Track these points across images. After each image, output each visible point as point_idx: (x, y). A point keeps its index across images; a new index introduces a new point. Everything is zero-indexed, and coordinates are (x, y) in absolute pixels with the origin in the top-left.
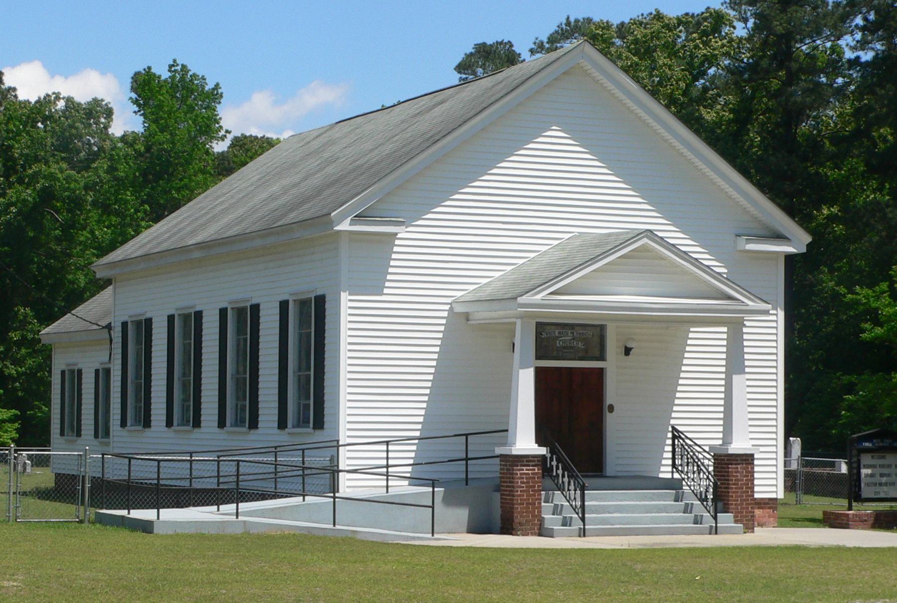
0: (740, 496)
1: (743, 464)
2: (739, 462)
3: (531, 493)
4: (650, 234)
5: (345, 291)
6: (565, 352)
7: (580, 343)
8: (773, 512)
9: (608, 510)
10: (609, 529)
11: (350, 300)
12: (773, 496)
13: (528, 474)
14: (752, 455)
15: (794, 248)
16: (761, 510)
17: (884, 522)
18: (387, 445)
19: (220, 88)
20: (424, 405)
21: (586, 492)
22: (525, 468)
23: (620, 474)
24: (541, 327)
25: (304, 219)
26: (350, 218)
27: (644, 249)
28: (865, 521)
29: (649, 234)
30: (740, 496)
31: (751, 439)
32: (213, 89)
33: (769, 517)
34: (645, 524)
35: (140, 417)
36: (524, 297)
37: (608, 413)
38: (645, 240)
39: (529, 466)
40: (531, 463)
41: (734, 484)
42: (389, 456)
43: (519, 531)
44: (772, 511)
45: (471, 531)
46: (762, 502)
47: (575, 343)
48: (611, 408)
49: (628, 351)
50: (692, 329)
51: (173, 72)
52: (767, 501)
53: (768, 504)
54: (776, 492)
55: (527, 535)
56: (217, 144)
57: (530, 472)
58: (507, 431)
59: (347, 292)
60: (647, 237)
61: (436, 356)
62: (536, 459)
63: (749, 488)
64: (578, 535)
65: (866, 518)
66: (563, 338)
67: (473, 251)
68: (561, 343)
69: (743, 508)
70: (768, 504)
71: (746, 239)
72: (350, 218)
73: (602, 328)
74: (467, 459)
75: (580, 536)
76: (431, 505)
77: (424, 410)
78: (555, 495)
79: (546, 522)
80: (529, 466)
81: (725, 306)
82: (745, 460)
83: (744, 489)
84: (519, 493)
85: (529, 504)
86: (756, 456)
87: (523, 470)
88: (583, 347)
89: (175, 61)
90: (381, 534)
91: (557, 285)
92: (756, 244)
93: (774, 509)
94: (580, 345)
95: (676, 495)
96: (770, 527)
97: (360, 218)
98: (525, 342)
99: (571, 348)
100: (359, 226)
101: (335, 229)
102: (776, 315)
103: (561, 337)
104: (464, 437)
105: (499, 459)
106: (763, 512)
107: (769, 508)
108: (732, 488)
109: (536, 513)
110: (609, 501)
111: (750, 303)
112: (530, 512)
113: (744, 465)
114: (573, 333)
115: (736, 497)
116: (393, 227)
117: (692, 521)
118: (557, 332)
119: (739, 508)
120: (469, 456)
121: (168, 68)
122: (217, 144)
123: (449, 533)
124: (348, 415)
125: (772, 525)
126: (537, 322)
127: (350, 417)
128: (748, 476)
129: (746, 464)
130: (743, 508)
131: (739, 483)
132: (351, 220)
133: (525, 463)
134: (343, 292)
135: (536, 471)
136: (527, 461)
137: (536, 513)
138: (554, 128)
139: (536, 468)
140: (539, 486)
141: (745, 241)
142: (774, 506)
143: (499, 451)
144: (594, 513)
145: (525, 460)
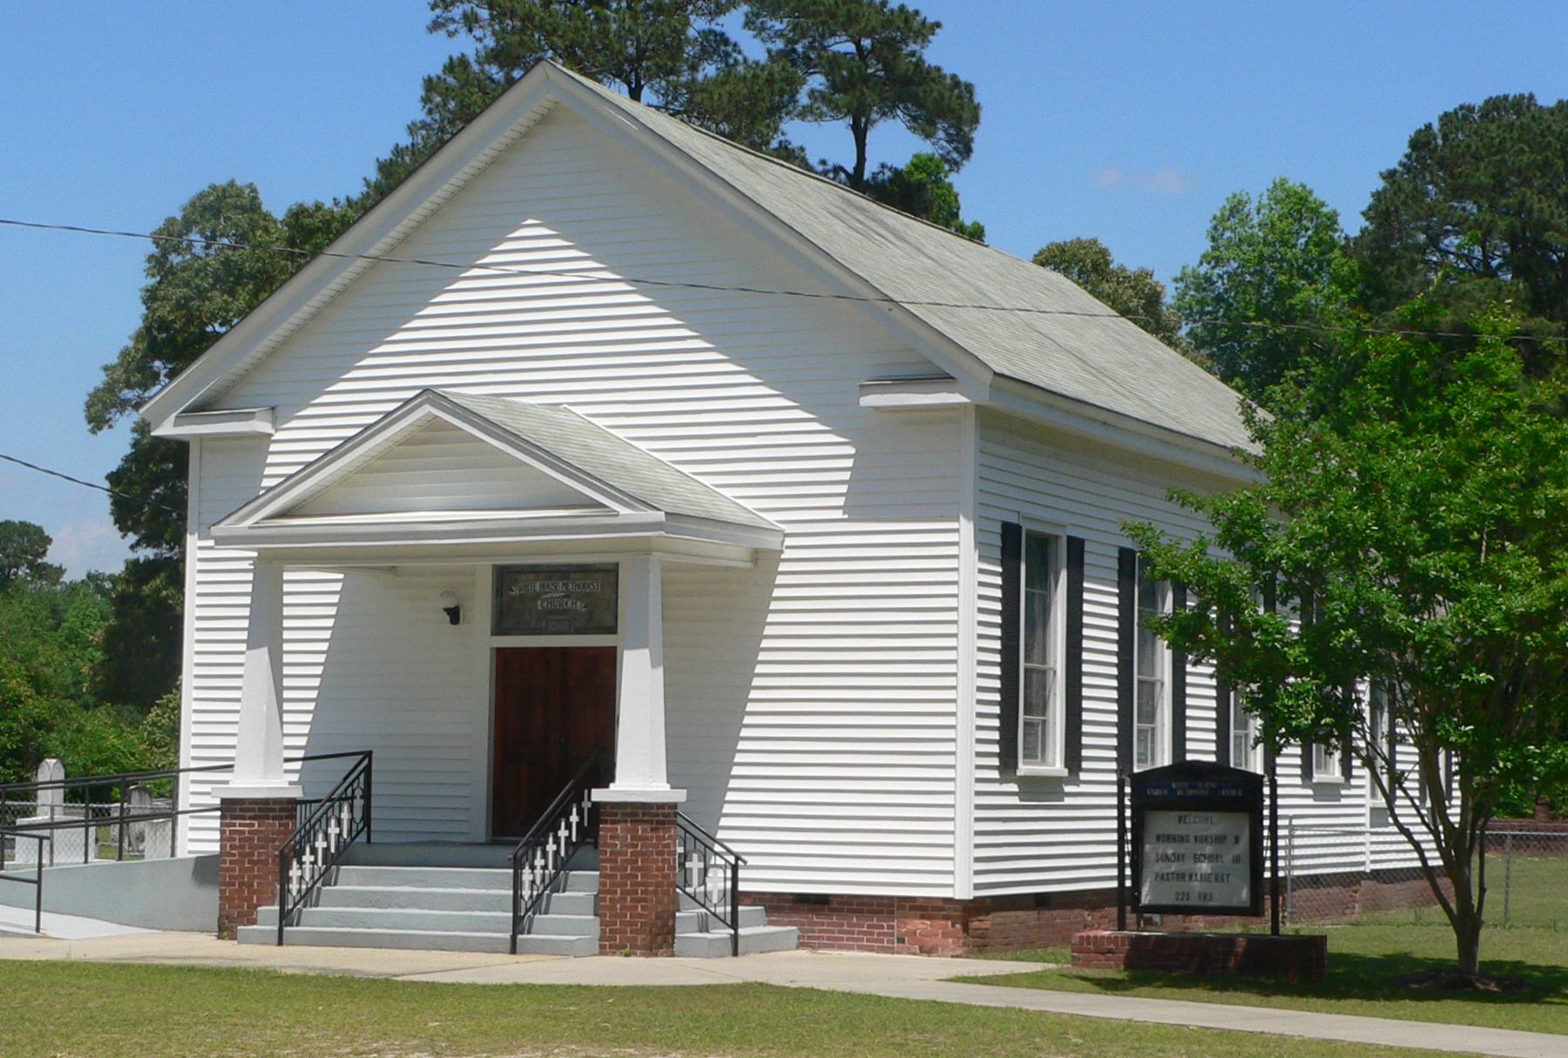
0: (619, 885)
1: (626, 821)
2: (619, 818)
3: (247, 865)
5: (192, 534)
7: (578, 603)
8: (953, 925)
11: (201, 548)
15: (965, 396)
22: (238, 822)
24: (505, 576)
25: (1053, 389)
26: (174, 415)
27: (433, 425)
28: (1110, 951)
33: (945, 935)
34: (426, 930)
35: (1237, 747)
36: (222, 525)
38: (427, 408)
39: (244, 818)
44: (950, 923)
46: (930, 905)
47: (570, 603)
50: (286, 576)
52: (940, 904)
53: (942, 909)
57: (246, 829)
59: (197, 535)
60: (428, 401)
62: (256, 807)
64: (509, 950)
65: (1112, 946)
68: (545, 604)
69: (627, 908)
70: (942, 909)
72: (174, 415)
76: (36, 878)
77: (309, 726)
78: (341, 872)
80: (244, 818)
81: (570, 520)
83: (629, 871)
84: (228, 865)
87: (234, 825)
88: (584, 610)
92: (882, 393)
96: (946, 956)
97: (201, 409)
98: (481, 610)
99: (564, 612)
100: (188, 427)
101: (153, 434)
106: (931, 926)
107: (946, 918)
110: (432, 887)
111: (623, 511)
113: (629, 824)
114: (566, 585)
118: (538, 584)
119: (618, 906)
125: (952, 953)
126: (495, 567)
127: (197, 737)
128: (637, 846)
129: (632, 821)
130: (627, 908)
131: (619, 859)
132: (177, 417)
133: (238, 813)
136: (241, 810)
138: (530, 221)
139: (256, 822)
144: (373, 906)
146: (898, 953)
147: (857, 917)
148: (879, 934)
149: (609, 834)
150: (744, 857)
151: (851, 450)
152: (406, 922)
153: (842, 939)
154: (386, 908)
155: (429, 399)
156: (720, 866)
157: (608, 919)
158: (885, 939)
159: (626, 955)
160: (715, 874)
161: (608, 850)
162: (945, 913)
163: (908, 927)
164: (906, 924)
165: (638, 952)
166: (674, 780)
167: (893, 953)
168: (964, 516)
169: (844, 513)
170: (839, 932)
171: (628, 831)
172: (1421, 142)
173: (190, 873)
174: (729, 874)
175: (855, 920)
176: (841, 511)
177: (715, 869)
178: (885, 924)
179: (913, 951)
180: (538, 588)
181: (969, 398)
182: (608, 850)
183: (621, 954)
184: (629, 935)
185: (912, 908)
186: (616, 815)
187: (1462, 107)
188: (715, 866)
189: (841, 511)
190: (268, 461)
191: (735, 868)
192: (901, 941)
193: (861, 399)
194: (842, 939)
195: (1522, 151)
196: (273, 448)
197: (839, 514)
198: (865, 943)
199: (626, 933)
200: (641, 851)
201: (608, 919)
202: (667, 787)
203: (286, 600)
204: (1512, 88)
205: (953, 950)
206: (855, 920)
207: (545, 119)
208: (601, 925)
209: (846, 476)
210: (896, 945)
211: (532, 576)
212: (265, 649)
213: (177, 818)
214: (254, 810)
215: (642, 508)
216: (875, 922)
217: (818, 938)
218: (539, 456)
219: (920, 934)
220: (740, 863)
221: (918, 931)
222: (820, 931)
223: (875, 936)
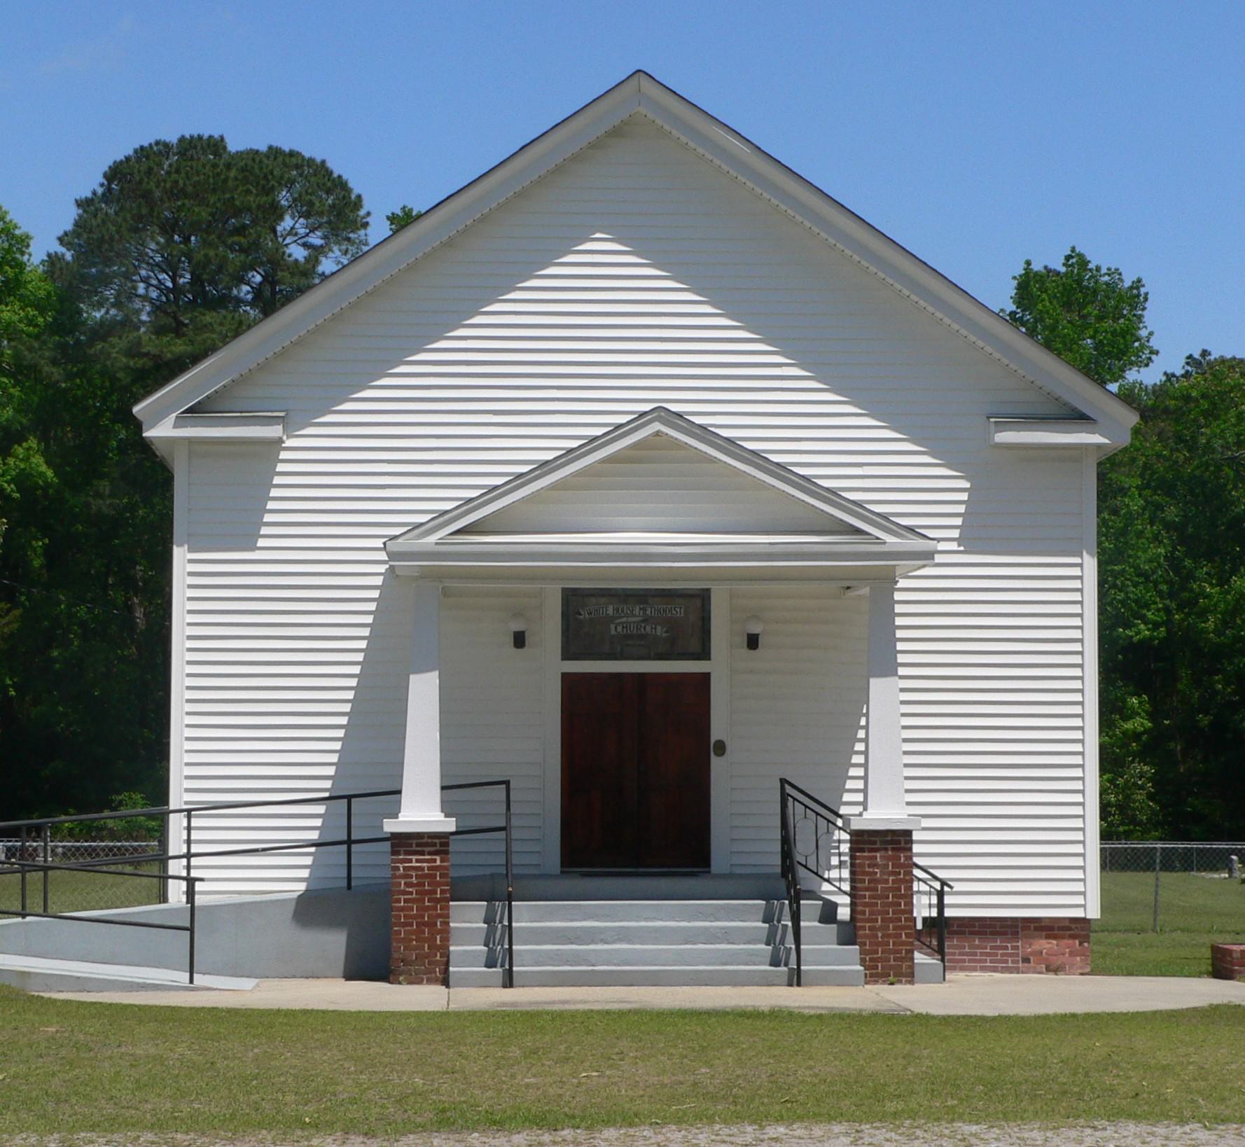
0: (880, 913)
1: (886, 849)
2: (878, 846)
4: (661, 414)
6: (628, 645)
7: (659, 628)
8: (1081, 944)
9: (602, 936)
10: (569, 972)
11: (190, 561)
12: (1078, 913)
13: (422, 869)
14: (908, 833)
15: (1105, 437)
16: (1055, 942)
17: (1222, 967)
18: (189, 818)
19: (1143, 286)
20: (337, 746)
21: (802, 902)
22: (414, 858)
23: (738, 871)
24: (574, 600)
26: (175, 415)
29: (663, 414)
30: (880, 913)
31: (909, 804)
32: (1131, 288)
33: (1072, 954)
37: (713, 757)
38: (657, 426)
40: (427, 849)
41: (867, 889)
42: (193, 837)
43: (401, 974)
44: (1077, 942)
45: (351, 974)
47: (648, 628)
48: (721, 748)
49: (753, 642)
51: (1070, 266)
52: (1067, 924)
53: (1070, 929)
54: (1084, 906)
55: (420, 982)
56: (1139, 371)
57: (425, 864)
58: (399, 792)
59: (186, 547)
61: (360, 657)
62: (437, 841)
63: (902, 896)
66: (624, 620)
67: (435, 465)
68: (620, 629)
69: (889, 936)
71: (995, 422)
73: (703, 597)
74: (349, 842)
75: (790, 985)
76: (188, 925)
79: (857, 957)
82: (892, 842)
83: (891, 899)
85: (425, 924)
86: (916, 836)
87: (411, 861)
88: (664, 635)
89: (1073, 250)
90: (79, 978)
91: (472, 515)
93: (1084, 939)
94: (659, 631)
95: (766, 909)
97: (197, 412)
98: (549, 632)
99: (641, 637)
102: (1081, 565)
103: (619, 618)
104: (346, 801)
105: (388, 844)
107: (1073, 937)
108: (864, 896)
109: (438, 942)
112: (425, 940)
113: (890, 853)
115: (871, 913)
116: (258, 427)
117: (768, 960)
118: (611, 608)
119: (880, 935)
120: (353, 838)
121: (1063, 261)
122: (1139, 371)
123: (307, 978)
124: (187, 764)
125: (1081, 971)
126: (563, 590)
129: (893, 849)
130: (889, 936)
132: (177, 417)
133: (414, 848)
134: (177, 546)
135: (438, 863)
137: (438, 942)
138: (598, 235)
139: (438, 858)
140: (442, 892)
141: (993, 426)
142: (1084, 933)
143: (390, 826)
144: (572, 943)
145: (414, 841)
146: (1023, 973)
147: (957, 938)
148: (1002, 955)
149: (867, 862)
150: (951, 883)
151: (967, 485)
152: (608, 958)
153: (964, 961)
154: (588, 944)
155: (661, 417)
156: (925, 893)
157: (867, 947)
158: (1010, 959)
159: (892, 984)
160: (919, 900)
161: (867, 878)
162: (1072, 932)
163: (1033, 947)
164: (1030, 945)
165: (904, 980)
166: (447, 809)
167: (1018, 973)
168: (1087, 553)
169: (959, 546)
170: (960, 954)
171: (889, 858)
172: (116, 173)
173: (291, 915)
174: (934, 900)
175: (977, 942)
176: (956, 543)
177: (919, 895)
178: (1009, 945)
179: (1039, 970)
180: (610, 611)
181: (1109, 439)
182: (867, 878)
183: (884, 982)
184: (892, 963)
185: (1036, 929)
186: (875, 843)
187: (157, 143)
188: (919, 892)
189: (956, 543)
190: (278, 469)
191: (941, 895)
192: (1026, 960)
193: (996, 435)
194: (964, 961)
195: (248, 192)
196: (283, 455)
197: (953, 546)
198: (988, 964)
199: (889, 961)
200: (904, 879)
201: (867, 947)
202: (440, 816)
203: (899, 621)
204: (207, 129)
205: (1081, 968)
206: (977, 942)
207: (617, 132)
208: (861, 954)
209: (961, 509)
210: (1020, 965)
211: (603, 600)
212: (436, 673)
213: (167, 863)
214: (435, 845)
215: (908, 535)
216: (955, 943)
217: (980, 961)
218: (793, 481)
219: (1046, 953)
220: (946, 889)
221: (1045, 951)
222: (982, 954)
223: (999, 957)
